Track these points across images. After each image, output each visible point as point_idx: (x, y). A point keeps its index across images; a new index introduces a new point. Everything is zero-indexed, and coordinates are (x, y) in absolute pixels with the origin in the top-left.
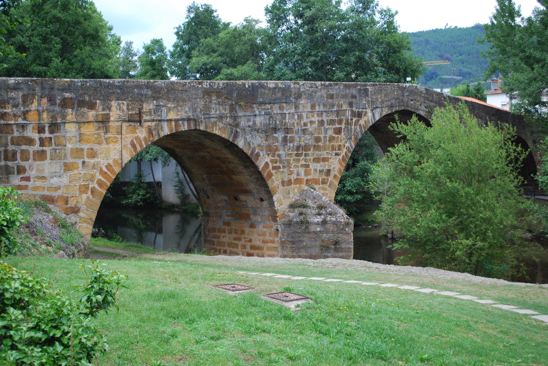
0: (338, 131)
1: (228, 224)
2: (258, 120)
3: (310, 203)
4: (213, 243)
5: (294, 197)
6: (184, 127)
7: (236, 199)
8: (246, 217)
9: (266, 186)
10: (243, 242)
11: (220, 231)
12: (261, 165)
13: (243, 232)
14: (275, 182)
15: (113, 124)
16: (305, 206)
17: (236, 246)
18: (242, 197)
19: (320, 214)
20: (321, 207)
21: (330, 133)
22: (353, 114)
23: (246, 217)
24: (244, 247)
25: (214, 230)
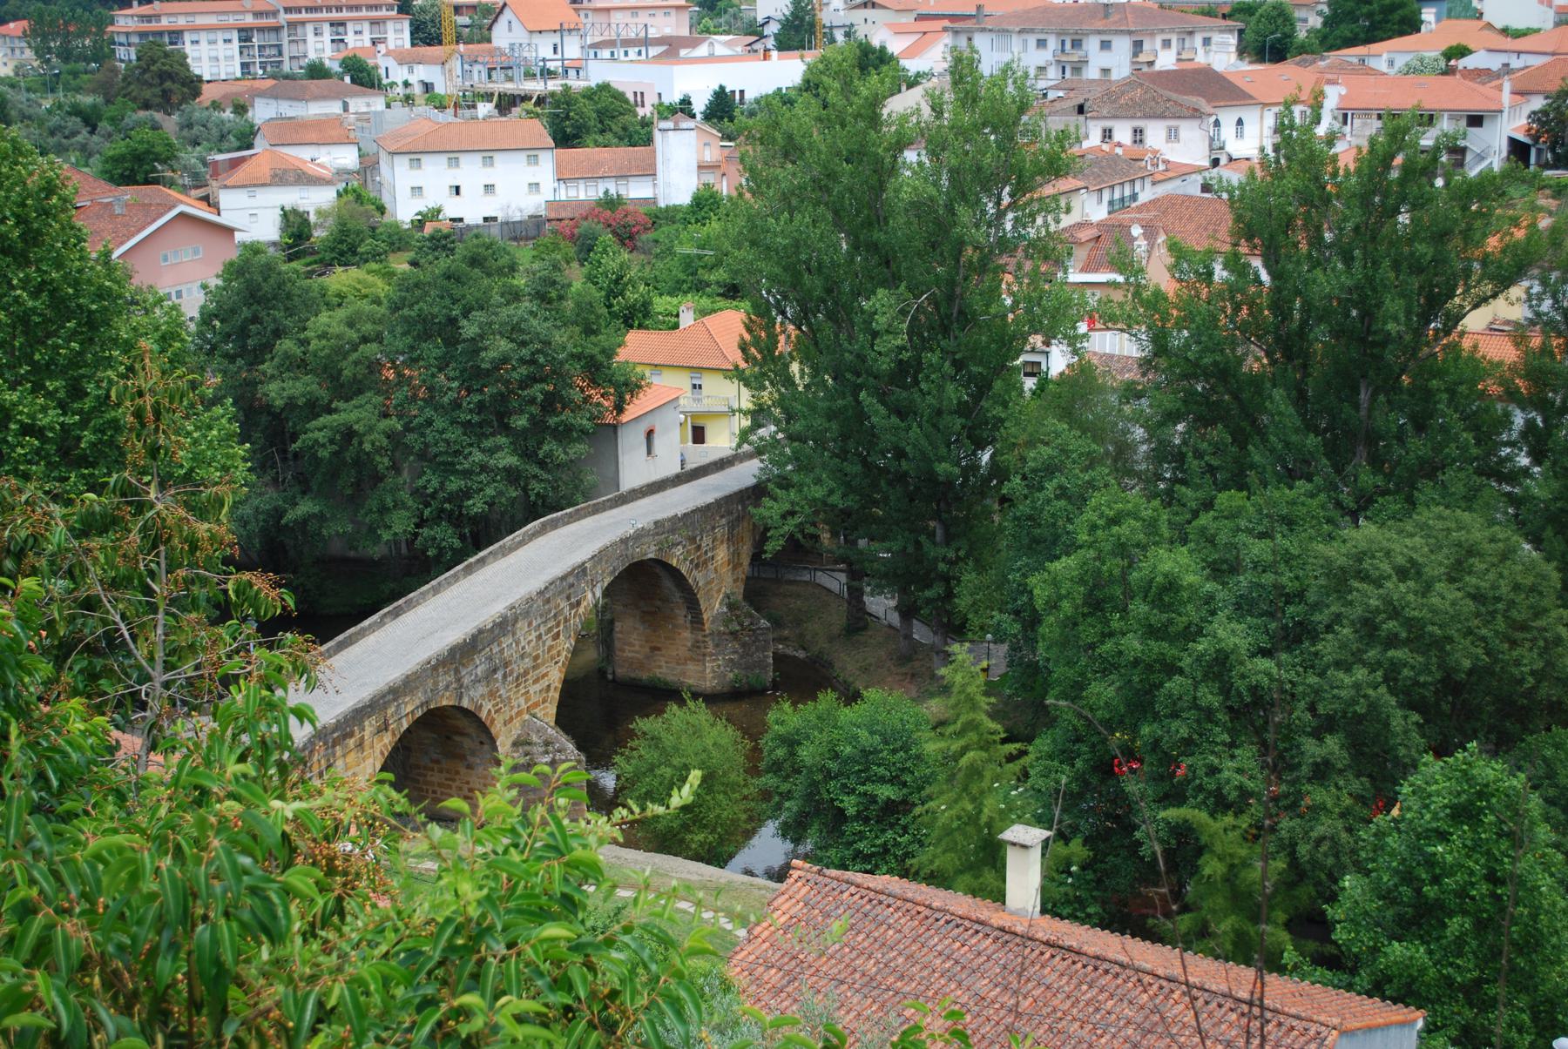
0: (557, 636)
1: (437, 762)
2: (479, 670)
3: (535, 738)
4: (418, 781)
5: (516, 730)
6: (419, 713)
7: (448, 738)
8: (462, 757)
9: (479, 720)
10: (458, 783)
11: (425, 768)
12: (483, 715)
13: (457, 773)
14: (497, 728)
15: (367, 743)
16: (529, 744)
17: (450, 787)
18: (457, 738)
19: (547, 752)
20: (547, 743)
21: (549, 643)
22: (572, 606)
23: (462, 757)
24: (460, 789)
25: (418, 767)
